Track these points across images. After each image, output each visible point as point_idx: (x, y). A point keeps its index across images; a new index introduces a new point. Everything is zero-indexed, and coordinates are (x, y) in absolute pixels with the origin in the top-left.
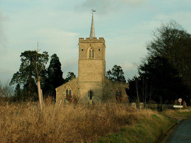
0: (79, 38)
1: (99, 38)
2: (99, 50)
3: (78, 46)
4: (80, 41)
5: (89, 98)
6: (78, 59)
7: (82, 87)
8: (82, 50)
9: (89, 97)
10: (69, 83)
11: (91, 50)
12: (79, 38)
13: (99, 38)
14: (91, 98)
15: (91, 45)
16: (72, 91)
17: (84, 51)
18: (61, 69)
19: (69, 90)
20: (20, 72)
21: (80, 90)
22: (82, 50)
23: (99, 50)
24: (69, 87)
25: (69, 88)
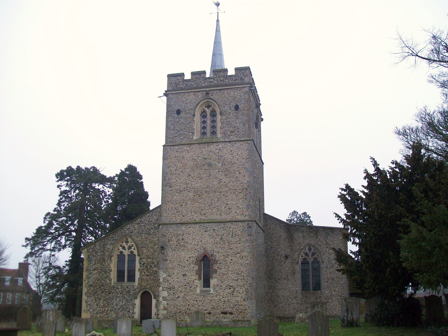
0: (169, 76)
1: (236, 69)
2: (237, 108)
3: (165, 98)
4: (169, 84)
5: (199, 283)
6: (164, 143)
7: (174, 241)
8: (178, 112)
9: (200, 279)
10: (128, 229)
11: (208, 111)
12: (169, 76)
13: (236, 69)
14: (207, 284)
15: (207, 94)
16: (137, 259)
17: (182, 114)
18: (138, 170)
19: (126, 253)
20: (352, 240)
21: (170, 253)
22: (178, 112)
23: (237, 108)
24: (127, 242)
25: (130, 248)
